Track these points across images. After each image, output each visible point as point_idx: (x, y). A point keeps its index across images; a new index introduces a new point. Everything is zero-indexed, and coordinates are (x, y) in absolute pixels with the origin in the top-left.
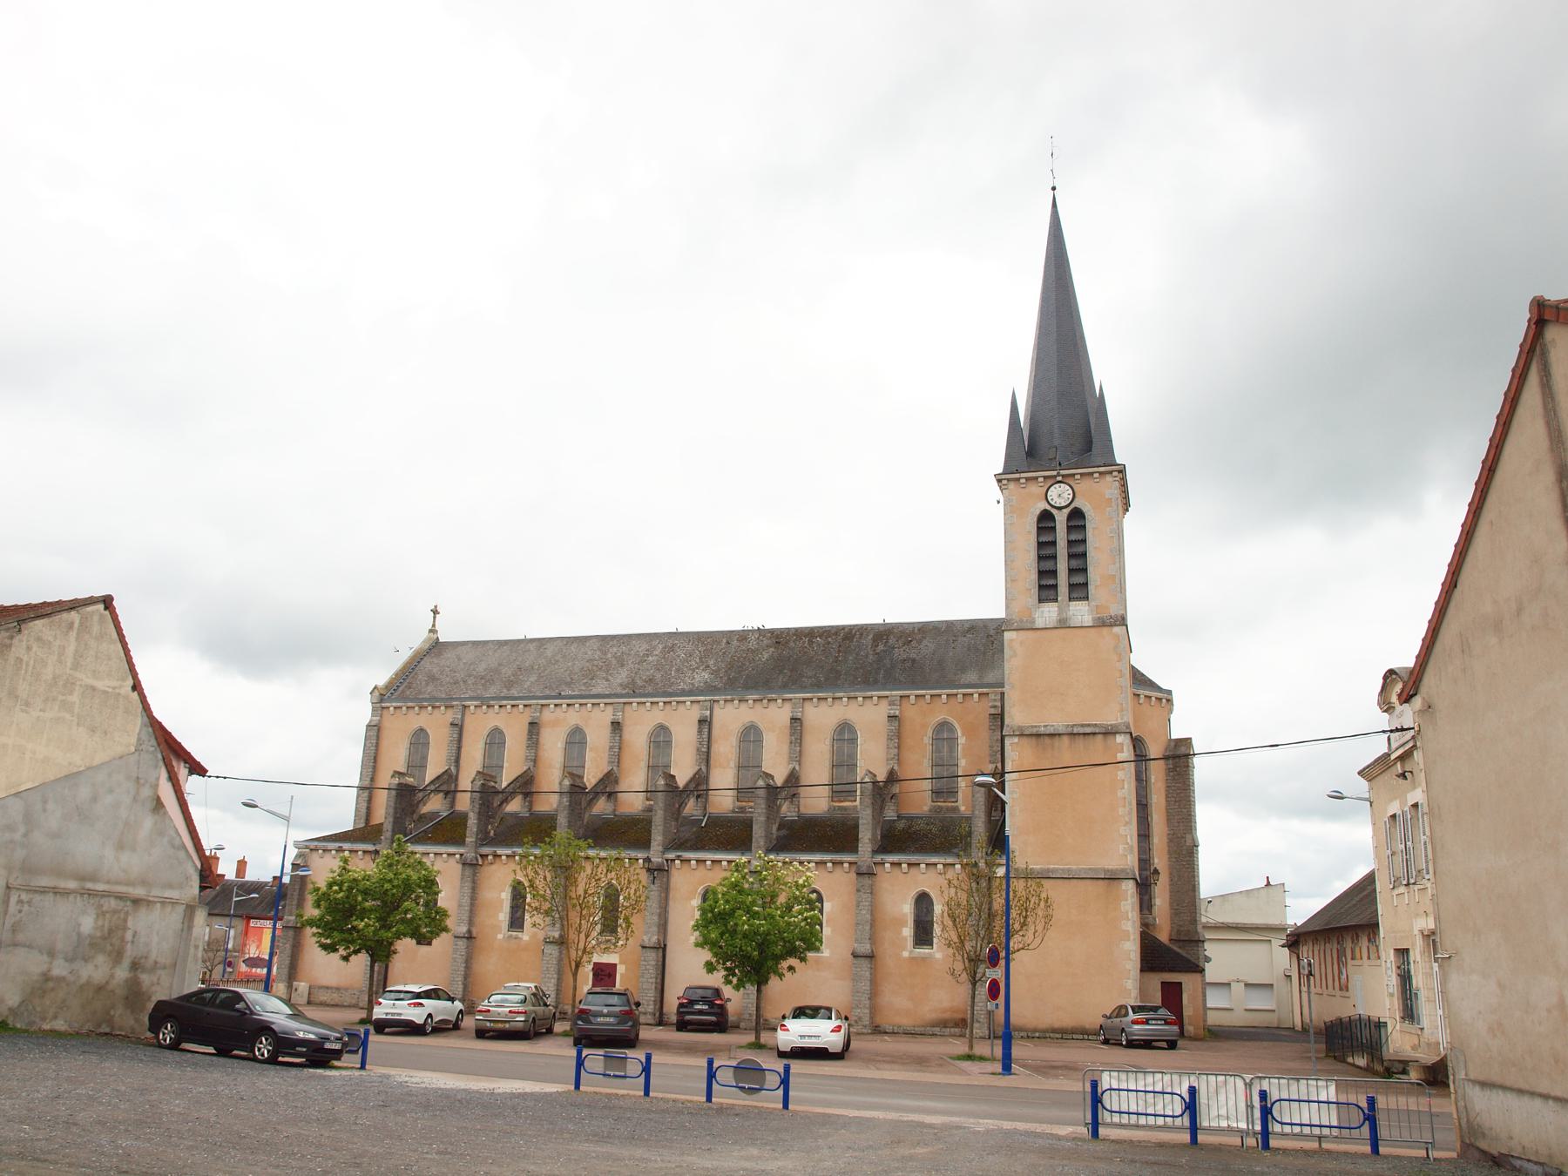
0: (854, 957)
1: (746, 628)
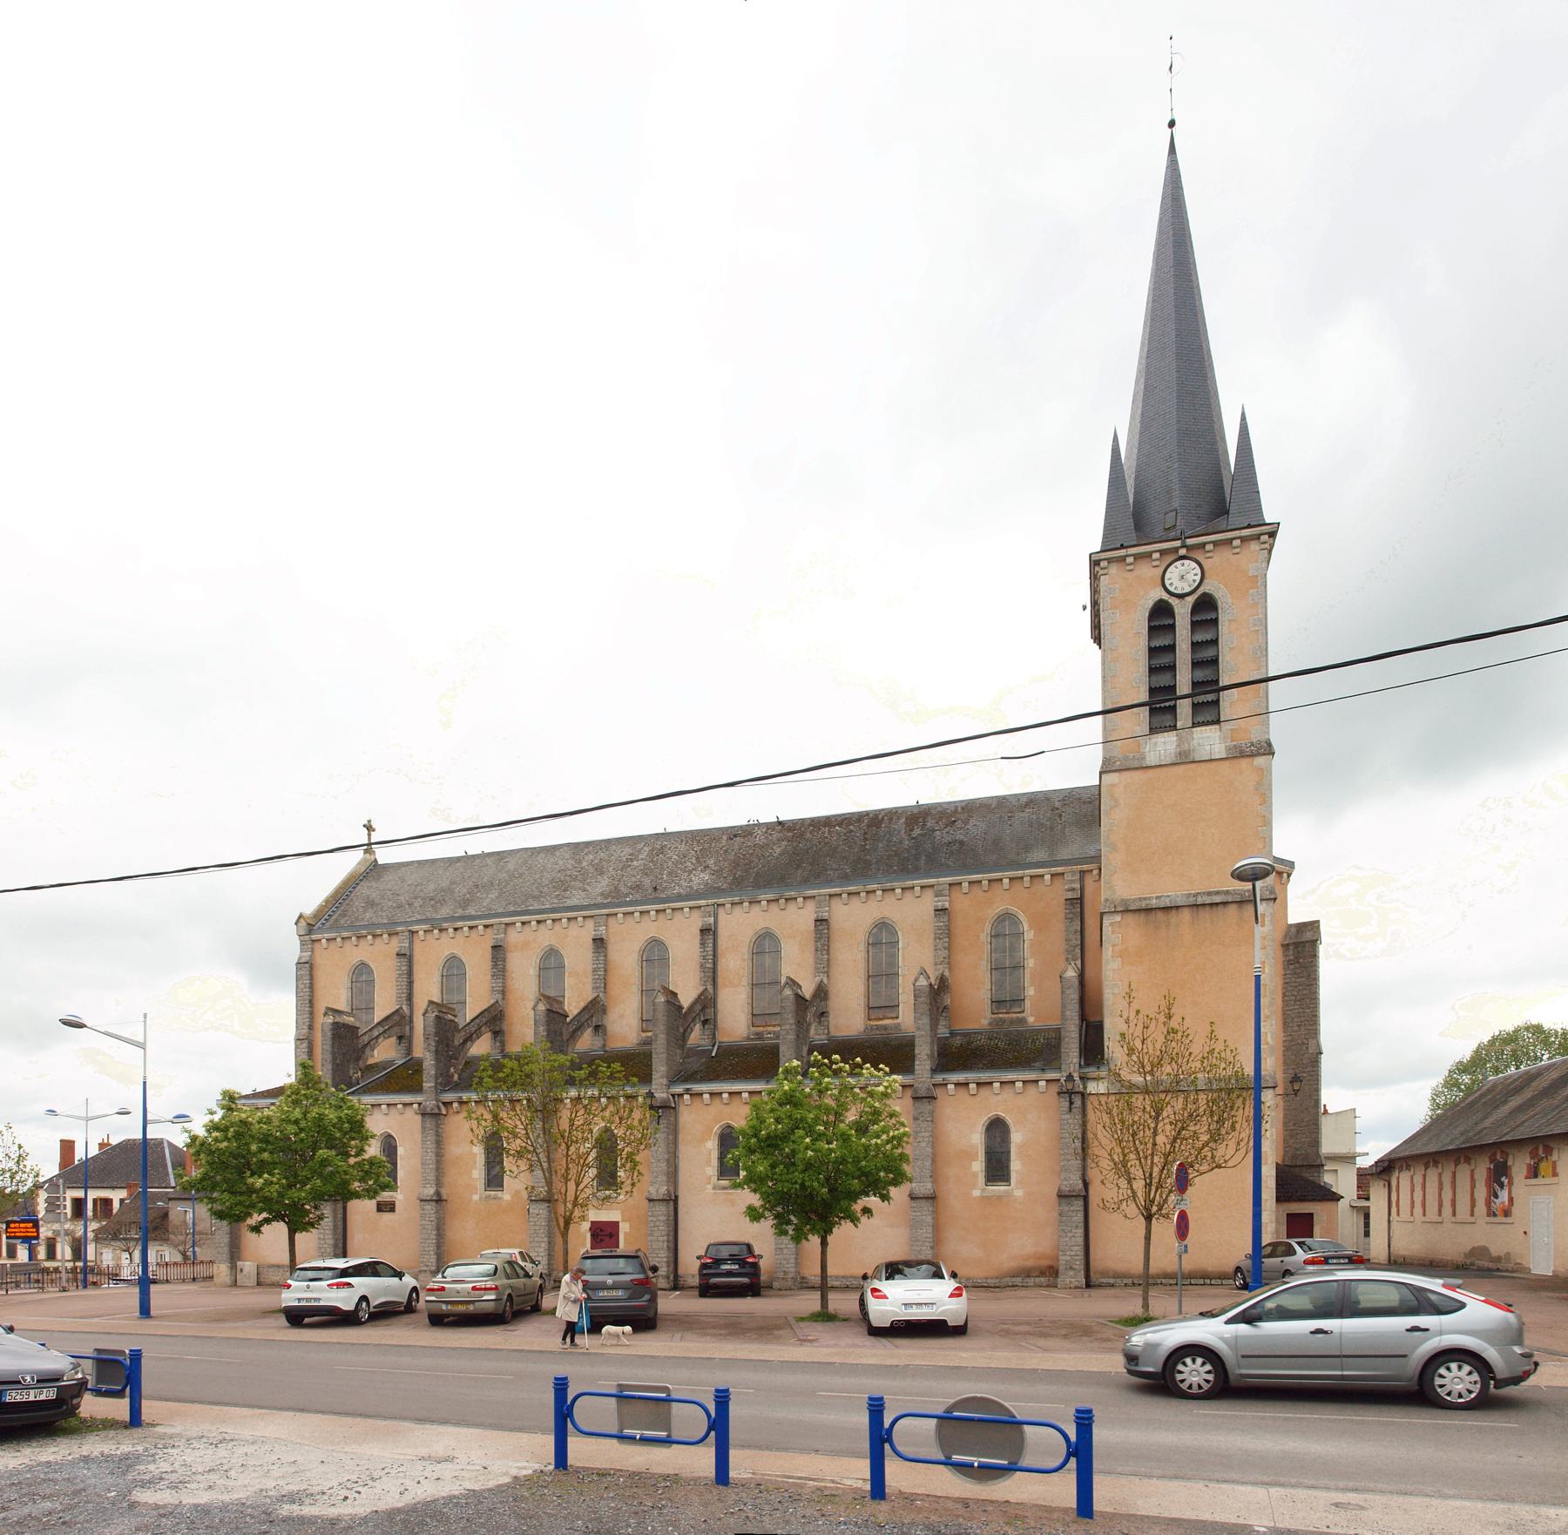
0: (912, 1198)
1: (751, 822)
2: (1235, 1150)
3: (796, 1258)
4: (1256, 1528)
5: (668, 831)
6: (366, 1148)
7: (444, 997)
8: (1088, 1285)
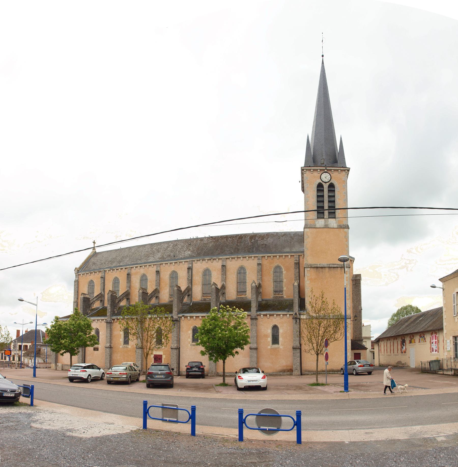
0: (250, 349)
2: (340, 335)
3: (215, 367)
4: (346, 442)
5: (178, 239)
6: (91, 332)
7: (113, 289)
8: (301, 374)
